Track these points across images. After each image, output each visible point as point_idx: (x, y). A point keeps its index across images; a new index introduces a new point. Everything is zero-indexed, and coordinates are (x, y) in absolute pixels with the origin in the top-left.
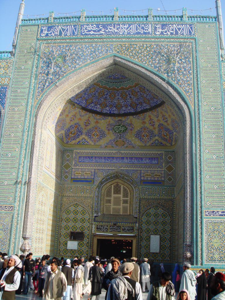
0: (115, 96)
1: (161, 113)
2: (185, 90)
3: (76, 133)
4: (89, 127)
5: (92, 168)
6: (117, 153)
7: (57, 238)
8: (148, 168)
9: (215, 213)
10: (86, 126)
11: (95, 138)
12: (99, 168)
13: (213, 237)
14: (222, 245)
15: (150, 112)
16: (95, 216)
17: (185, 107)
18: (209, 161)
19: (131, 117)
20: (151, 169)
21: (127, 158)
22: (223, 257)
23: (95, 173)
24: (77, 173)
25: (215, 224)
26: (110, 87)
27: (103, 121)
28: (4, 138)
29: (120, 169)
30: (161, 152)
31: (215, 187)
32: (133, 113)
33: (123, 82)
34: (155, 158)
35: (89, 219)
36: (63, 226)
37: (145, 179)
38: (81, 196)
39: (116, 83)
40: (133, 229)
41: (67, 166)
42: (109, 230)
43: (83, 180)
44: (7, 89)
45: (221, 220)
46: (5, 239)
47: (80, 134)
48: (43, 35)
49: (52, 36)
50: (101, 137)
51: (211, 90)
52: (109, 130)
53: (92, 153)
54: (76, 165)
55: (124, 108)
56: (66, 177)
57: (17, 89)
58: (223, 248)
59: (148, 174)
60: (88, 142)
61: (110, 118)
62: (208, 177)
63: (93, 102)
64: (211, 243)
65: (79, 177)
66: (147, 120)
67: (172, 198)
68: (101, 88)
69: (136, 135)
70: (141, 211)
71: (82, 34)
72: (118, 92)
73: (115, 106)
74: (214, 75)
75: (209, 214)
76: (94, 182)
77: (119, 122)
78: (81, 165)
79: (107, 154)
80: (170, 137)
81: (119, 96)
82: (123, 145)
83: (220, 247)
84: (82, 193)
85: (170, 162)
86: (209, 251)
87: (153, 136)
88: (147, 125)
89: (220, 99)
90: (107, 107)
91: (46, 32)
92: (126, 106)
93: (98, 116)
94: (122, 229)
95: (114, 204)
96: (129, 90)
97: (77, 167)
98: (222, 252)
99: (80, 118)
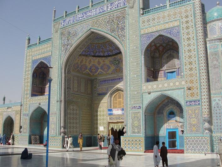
4: (101, 65)
42: (115, 119)
48: (109, 9)
49: (113, 9)
51: (134, 36)
52: (111, 64)
71: (77, 21)
82: (120, 71)
91: (110, 7)
97: (100, 87)
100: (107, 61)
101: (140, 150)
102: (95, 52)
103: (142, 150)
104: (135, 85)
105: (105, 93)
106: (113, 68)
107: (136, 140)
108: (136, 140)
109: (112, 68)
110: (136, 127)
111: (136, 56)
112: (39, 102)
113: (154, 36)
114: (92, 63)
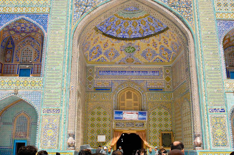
0: (128, 24)
5: (110, 79)
8: (152, 79)
10: (105, 47)
12: (115, 79)
15: (154, 37)
17: (189, 32)
18: (209, 72)
19: (139, 41)
20: (154, 80)
21: (136, 72)
22: (225, 143)
24: (98, 84)
25: (217, 118)
28: (49, 56)
29: (132, 80)
30: (161, 67)
32: (140, 38)
36: (89, 124)
37: (150, 87)
39: (130, 14)
41: (90, 78)
43: (103, 88)
44: (48, 17)
46: (55, 136)
50: (116, 56)
51: (207, 19)
52: (122, 51)
54: (97, 77)
55: (134, 34)
57: (56, 17)
58: (224, 136)
61: (122, 41)
62: (209, 83)
64: (216, 133)
65: (100, 87)
67: (171, 101)
68: (118, 18)
72: (131, 21)
74: (209, 8)
75: (212, 111)
78: (101, 78)
81: (131, 25)
82: (133, 62)
84: (103, 99)
85: (168, 74)
86: (215, 139)
88: (151, 47)
89: (215, 26)
92: (136, 32)
96: (139, 20)
97: (98, 79)
98: (224, 139)
100: (118, 45)
102: (109, 28)
104: (213, 80)
109: (121, 55)
110: (220, 137)
114: (98, 43)
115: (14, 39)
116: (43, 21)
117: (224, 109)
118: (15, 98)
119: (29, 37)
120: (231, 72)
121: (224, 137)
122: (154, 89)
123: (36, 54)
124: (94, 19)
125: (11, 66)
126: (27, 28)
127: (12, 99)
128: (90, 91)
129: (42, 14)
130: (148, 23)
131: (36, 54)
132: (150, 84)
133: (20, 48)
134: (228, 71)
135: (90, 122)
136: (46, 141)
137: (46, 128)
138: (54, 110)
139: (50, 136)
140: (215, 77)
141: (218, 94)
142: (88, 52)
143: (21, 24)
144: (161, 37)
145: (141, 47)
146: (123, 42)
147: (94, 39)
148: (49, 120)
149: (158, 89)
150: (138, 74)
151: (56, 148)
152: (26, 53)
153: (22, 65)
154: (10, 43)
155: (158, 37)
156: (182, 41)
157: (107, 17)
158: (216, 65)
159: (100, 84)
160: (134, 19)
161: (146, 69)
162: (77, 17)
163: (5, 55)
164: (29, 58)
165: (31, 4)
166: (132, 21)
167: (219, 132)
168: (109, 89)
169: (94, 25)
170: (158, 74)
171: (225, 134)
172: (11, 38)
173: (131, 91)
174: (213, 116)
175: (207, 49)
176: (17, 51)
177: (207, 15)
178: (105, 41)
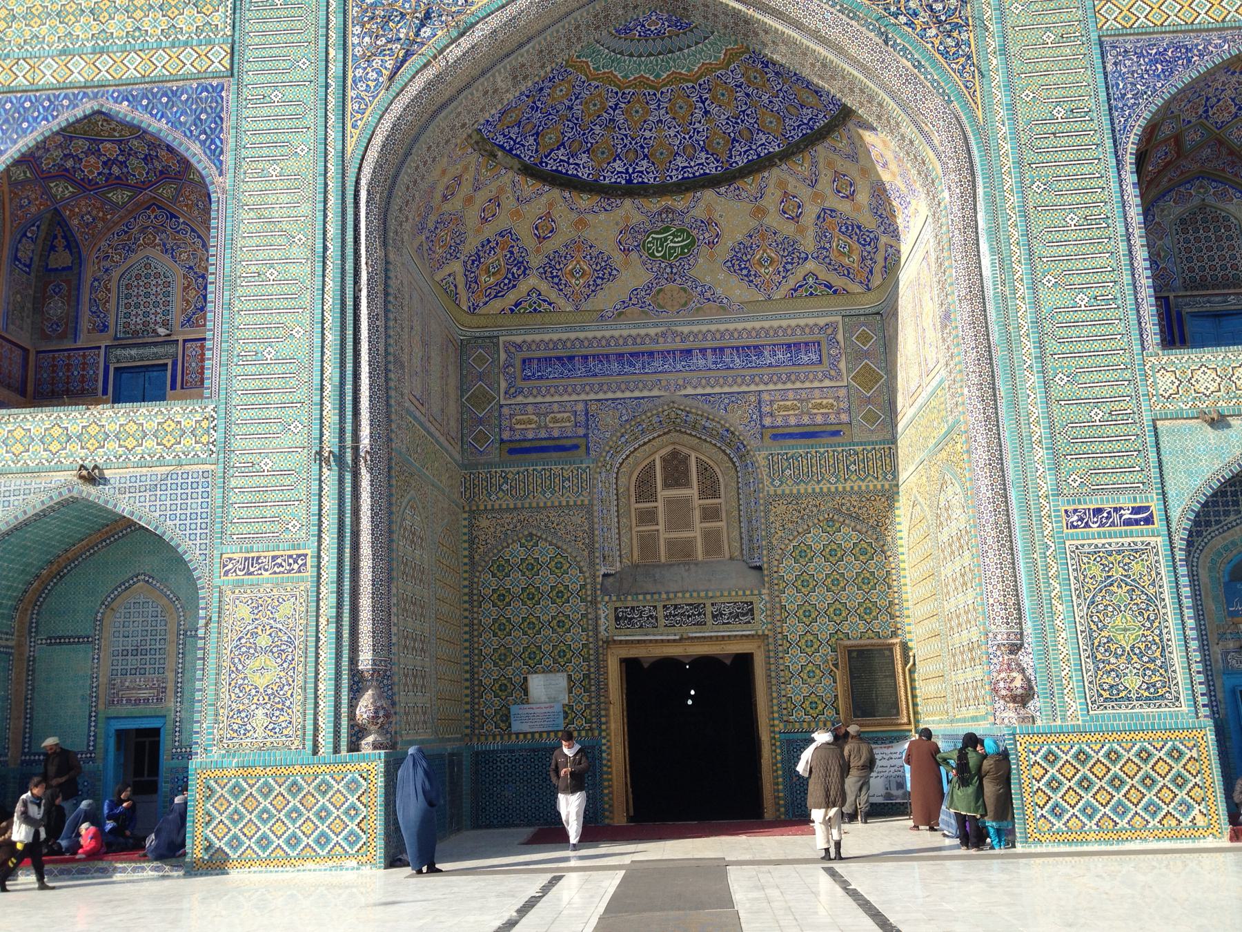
1: (830, 164)
2: (941, 48)
3: (504, 271)
4: (550, 246)
5: (574, 397)
6: (664, 334)
7: (467, 668)
9: (1105, 515)
10: (541, 239)
11: (578, 283)
13: (1110, 609)
14: (1150, 638)
15: (784, 167)
16: (605, 575)
19: (708, 195)
20: (798, 385)
23: (586, 414)
24: (519, 422)
26: (626, 77)
27: (602, 216)
29: (684, 392)
31: (1097, 414)
33: (680, 49)
34: (806, 344)
35: (583, 587)
37: (779, 422)
38: (545, 507)
39: (651, 54)
40: (752, 610)
42: (662, 622)
43: (544, 443)
44: (223, 94)
45: (1135, 539)
46: (286, 688)
47: (520, 272)
50: (599, 281)
51: (1050, 37)
53: (569, 344)
56: (481, 438)
57: (268, 91)
58: (1154, 647)
59: (789, 403)
60: (550, 304)
61: (628, 202)
63: (563, 144)
65: (530, 435)
66: (771, 201)
67: (887, 486)
68: (594, 83)
69: (729, 264)
70: (775, 542)
72: (659, 95)
73: (646, 156)
75: (1081, 519)
76: (588, 448)
77: (664, 216)
79: (625, 344)
80: (863, 259)
81: (662, 112)
82: (686, 304)
83: (1143, 647)
84: (548, 495)
85: (866, 355)
86: (1101, 665)
87: (796, 260)
90: (615, 160)
93: (585, 196)
94: (709, 616)
95: (670, 527)
96: (701, 81)
97: (520, 399)
98: (1152, 666)
99: (517, 211)
100: (606, 224)
101: (1186, 822)
103: (1201, 821)
104: (1082, 362)
105: (568, 443)
106: (633, 275)
107: (1144, 755)
108: (1143, 750)
111: (1067, 170)
112: (77, 454)
113: (1201, 55)
114: (503, 221)
115: (76, 222)
116: (203, 117)
117: (1148, 508)
118: (90, 514)
119: (154, 205)
120: (1194, 315)
121: (1151, 654)
122: (797, 430)
123: (193, 293)
124: (460, 92)
125: (69, 357)
126: (135, 162)
127: (79, 518)
128: (483, 459)
129: (195, 85)
130: (747, 95)
131: (193, 293)
132: (775, 406)
133: (107, 264)
134: (1179, 314)
135: (489, 613)
136: (243, 715)
137: (244, 649)
138: (279, 561)
139: (261, 690)
140: (1096, 346)
141: (1111, 431)
142: (457, 267)
143: (102, 141)
144: (821, 165)
145: (722, 222)
146: (629, 210)
147: (481, 198)
148: (256, 609)
149: (817, 429)
150: (715, 363)
151: (296, 743)
152: (142, 291)
153: (124, 347)
154: (60, 243)
155: (802, 165)
156: (919, 174)
157: (525, 78)
158: (1097, 278)
159: (530, 422)
160: (677, 78)
161: (754, 334)
162: (372, 84)
163: (39, 303)
164: (137, 315)
165: (137, 34)
166: (664, 90)
167: (1125, 629)
168: (576, 447)
169: (464, 125)
170: (815, 357)
171: (1157, 639)
172: (58, 220)
173: (686, 451)
174: (1086, 549)
175: (1049, 199)
176: (96, 284)
177: (1047, 19)
178: (537, 208)
